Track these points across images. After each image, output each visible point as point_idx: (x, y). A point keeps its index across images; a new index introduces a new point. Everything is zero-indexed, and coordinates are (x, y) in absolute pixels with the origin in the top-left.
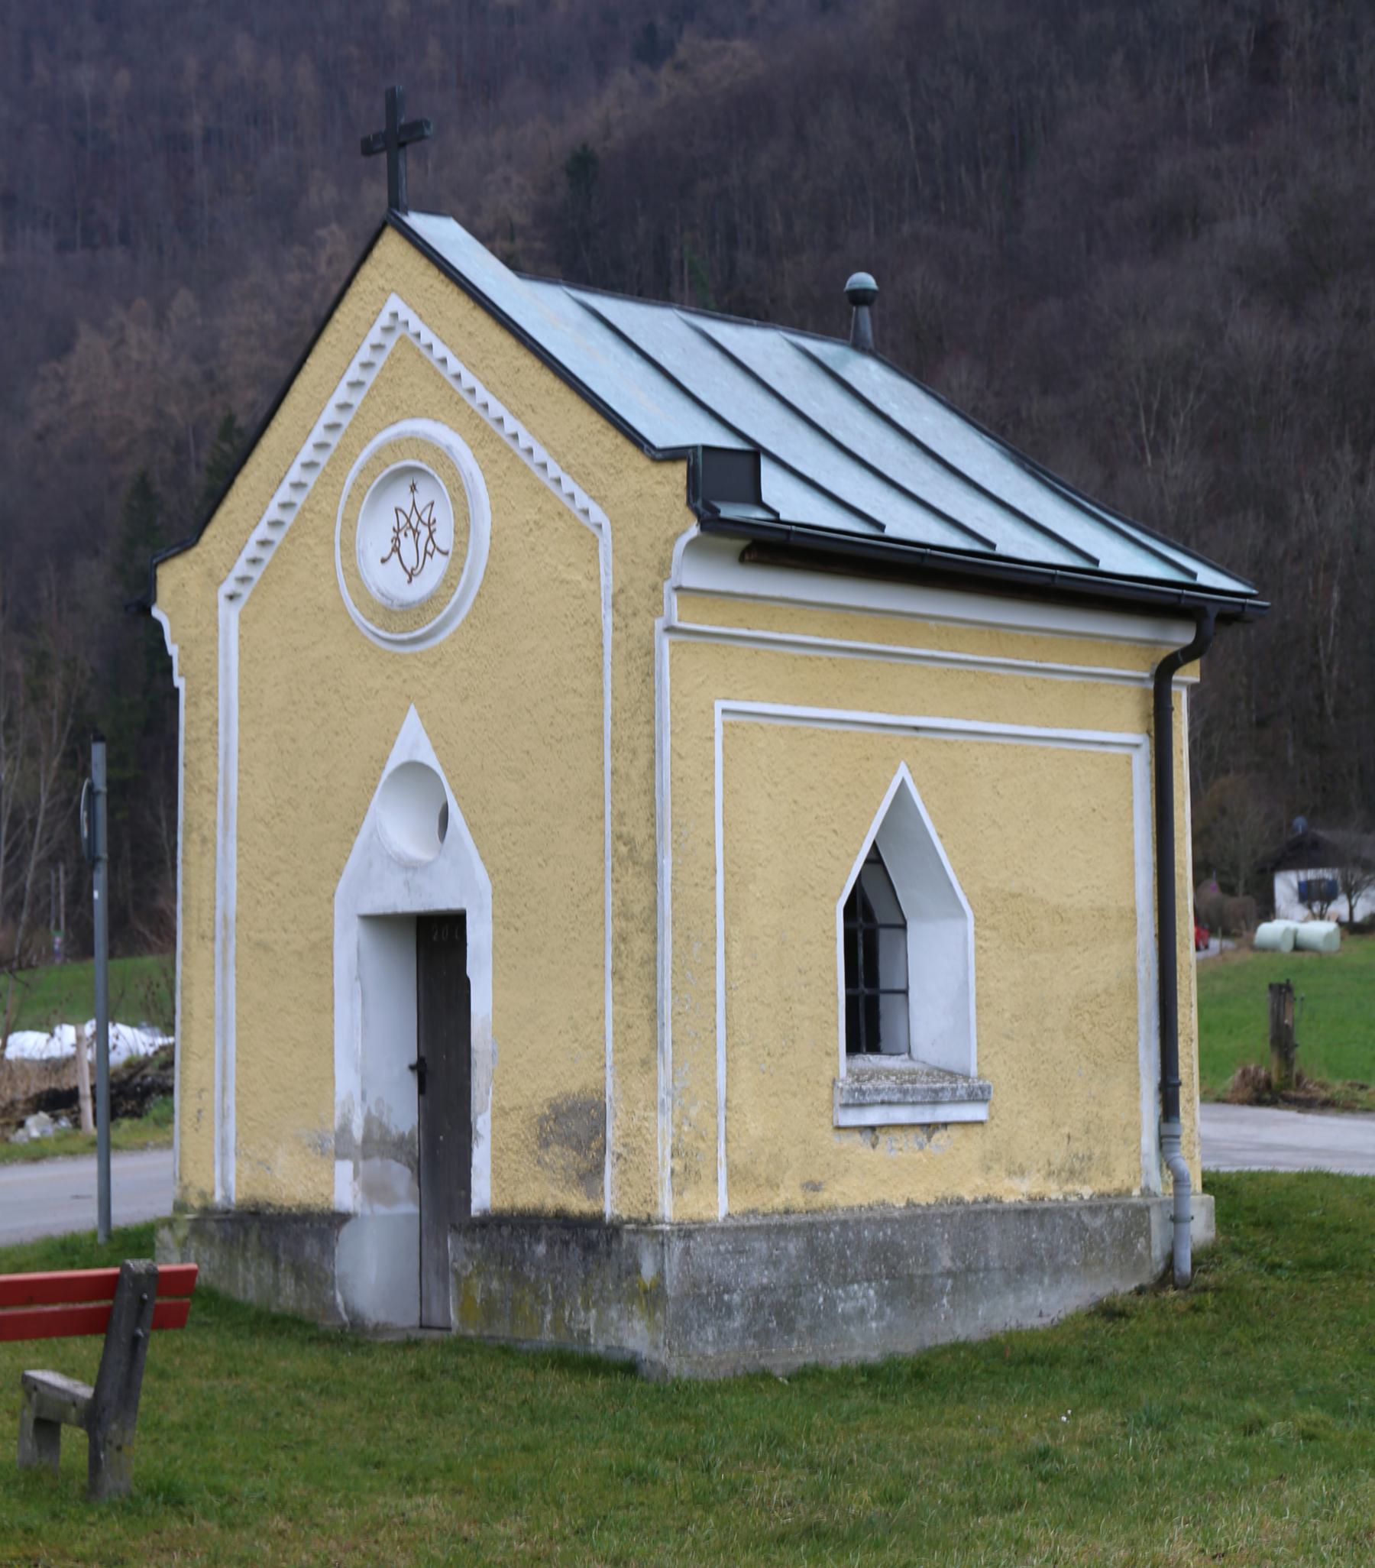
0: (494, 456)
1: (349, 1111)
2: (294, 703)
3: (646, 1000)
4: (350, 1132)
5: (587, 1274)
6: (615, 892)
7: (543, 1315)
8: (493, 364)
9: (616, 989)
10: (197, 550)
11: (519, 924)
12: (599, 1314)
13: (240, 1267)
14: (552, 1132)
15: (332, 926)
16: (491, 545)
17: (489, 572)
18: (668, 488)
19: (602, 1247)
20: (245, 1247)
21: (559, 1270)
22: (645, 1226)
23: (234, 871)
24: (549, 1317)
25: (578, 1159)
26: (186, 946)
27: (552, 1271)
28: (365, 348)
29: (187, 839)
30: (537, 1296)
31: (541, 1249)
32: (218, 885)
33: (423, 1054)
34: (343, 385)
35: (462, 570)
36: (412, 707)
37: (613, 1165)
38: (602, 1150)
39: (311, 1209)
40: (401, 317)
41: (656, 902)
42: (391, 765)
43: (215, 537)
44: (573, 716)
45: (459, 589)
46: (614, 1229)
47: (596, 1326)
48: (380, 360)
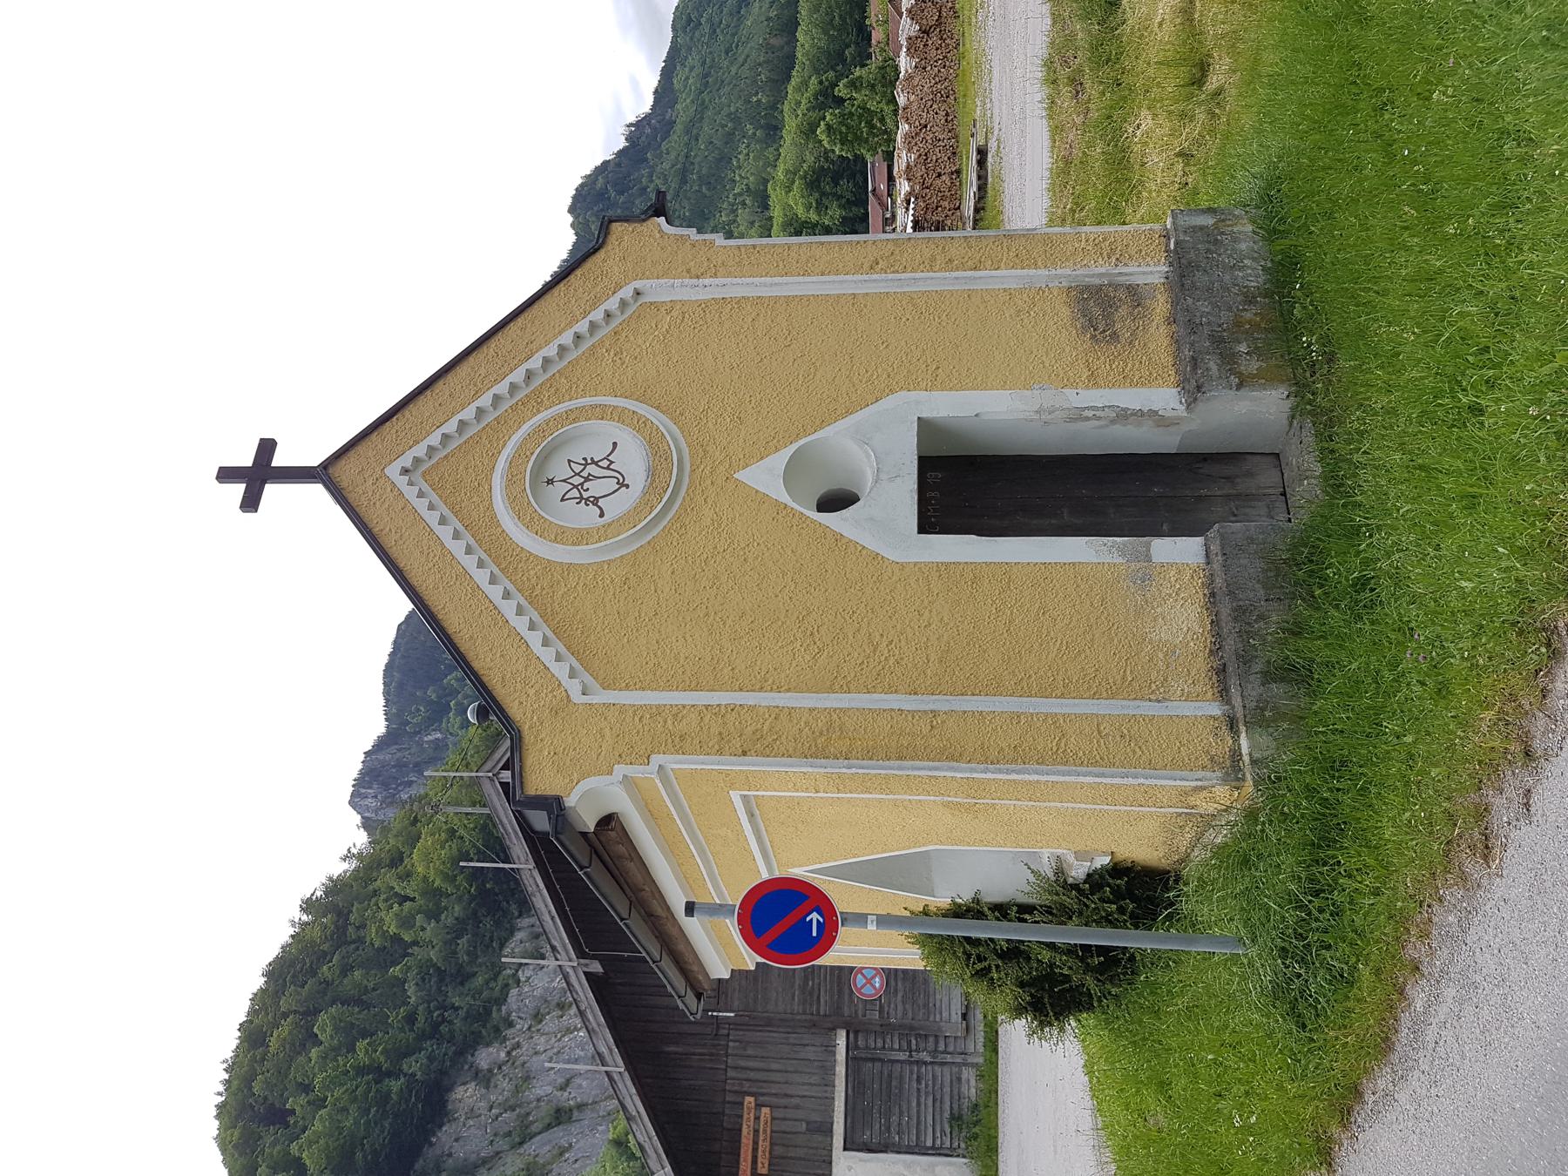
16: (621, 396)
40: (408, 464)
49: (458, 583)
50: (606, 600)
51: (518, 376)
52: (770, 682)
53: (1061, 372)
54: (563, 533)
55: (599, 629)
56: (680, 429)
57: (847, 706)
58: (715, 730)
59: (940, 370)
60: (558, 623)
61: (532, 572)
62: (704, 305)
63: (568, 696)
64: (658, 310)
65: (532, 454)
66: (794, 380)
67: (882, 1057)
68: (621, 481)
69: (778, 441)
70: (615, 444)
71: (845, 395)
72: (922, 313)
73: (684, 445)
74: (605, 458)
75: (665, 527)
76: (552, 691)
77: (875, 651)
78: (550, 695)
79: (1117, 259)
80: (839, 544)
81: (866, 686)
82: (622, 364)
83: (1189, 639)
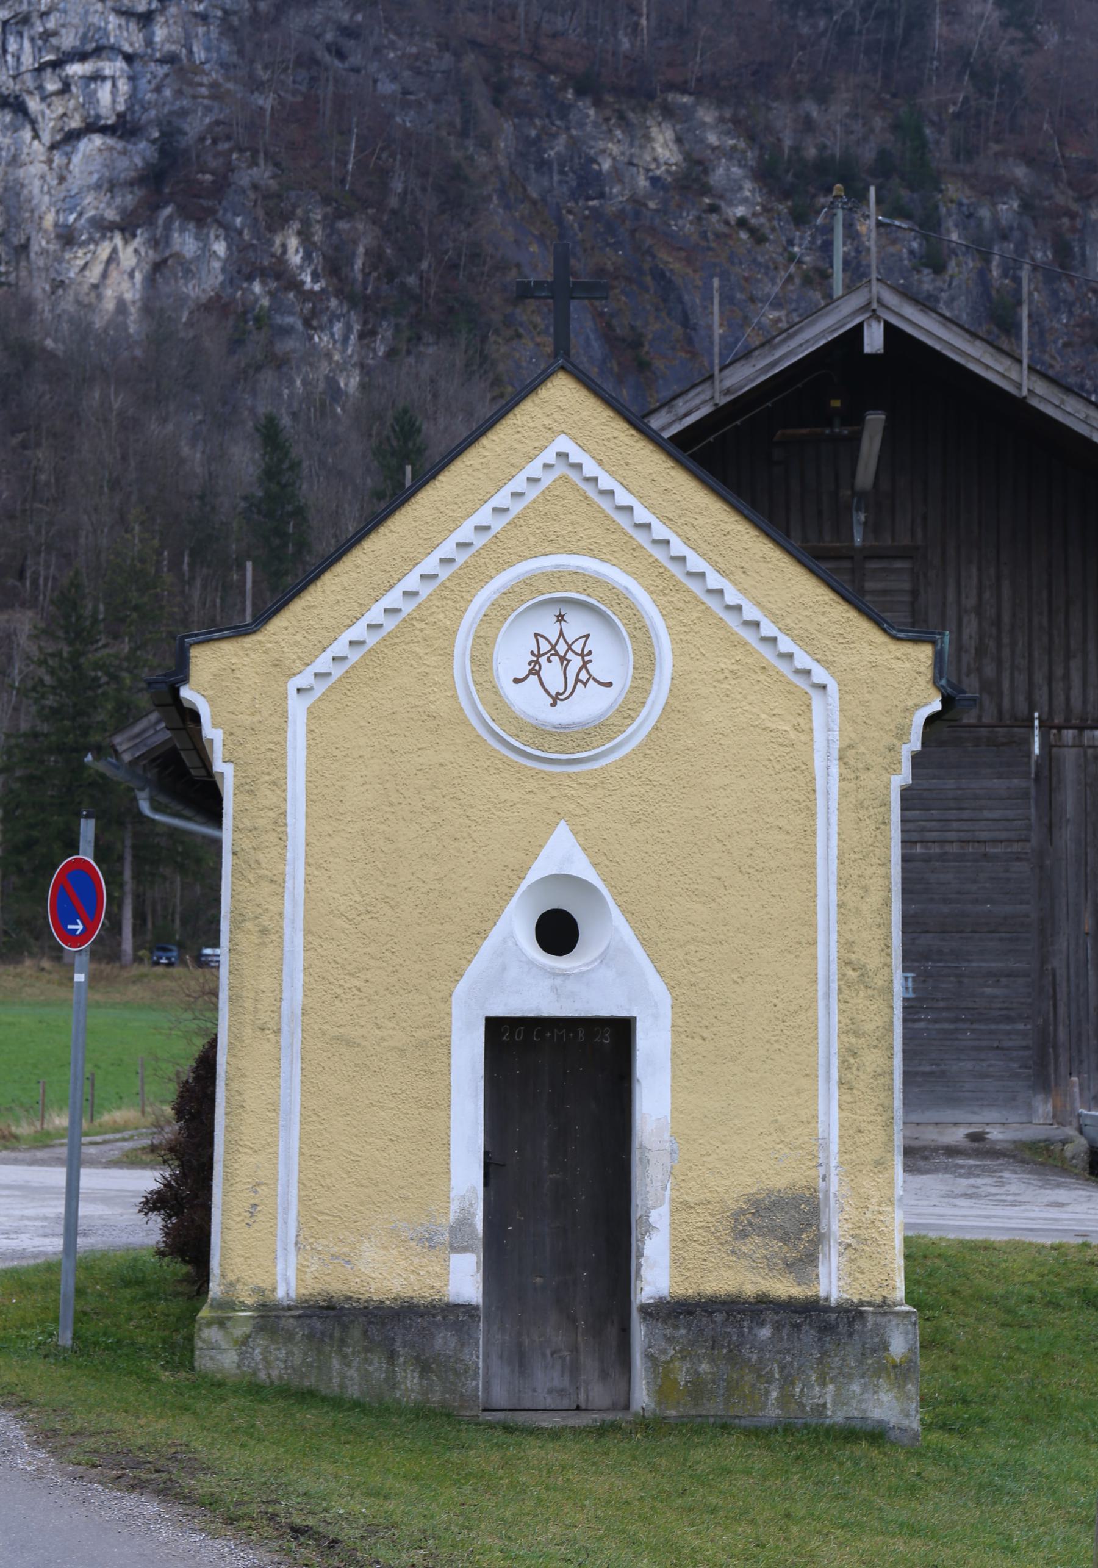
0: (681, 605)
1: (471, 1205)
2: (391, 804)
3: (880, 1108)
5: (824, 1353)
6: (841, 1012)
7: (767, 1393)
8: (695, 523)
9: (844, 1097)
12: (838, 1389)
13: (336, 1363)
14: (751, 1224)
15: (449, 1025)
16: (673, 684)
17: (667, 708)
18: (908, 665)
19: (842, 1328)
20: (342, 1341)
21: (788, 1351)
25: (785, 1249)
27: (779, 1352)
28: (521, 478)
30: (759, 1376)
31: (765, 1333)
34: (487, 508)
35: (644, 703)
36: (562, 823)
37: (841, 1255)
38: (819, 1240)
39: (415, 1301)
43: (286, 628)
45: (638, 721)
47: (834, 1401)
48: (533, 493)
49: (421, 541)
50: (410, 699)
51: (696, 563)
52: (316, 873)
53: (694, 1174)
55: (375, 694)
56: (627, 756)
57: (286, 949)
58: (260, 823)
59: (701, 1041)
61: (441, 616)
62: (805, 769)
63: (294, 675)
65: (588, 595)
69: (607, 866)
70: (609, 684)
71: (667, 936)
73: (603, 762)
75: (498, 752)
76: (300, 658)
77: (350, 974)
78: (295, 657)
79: (850, 1245)
80: (474, 936)
82: (719, 681)
83: (363, 1278)
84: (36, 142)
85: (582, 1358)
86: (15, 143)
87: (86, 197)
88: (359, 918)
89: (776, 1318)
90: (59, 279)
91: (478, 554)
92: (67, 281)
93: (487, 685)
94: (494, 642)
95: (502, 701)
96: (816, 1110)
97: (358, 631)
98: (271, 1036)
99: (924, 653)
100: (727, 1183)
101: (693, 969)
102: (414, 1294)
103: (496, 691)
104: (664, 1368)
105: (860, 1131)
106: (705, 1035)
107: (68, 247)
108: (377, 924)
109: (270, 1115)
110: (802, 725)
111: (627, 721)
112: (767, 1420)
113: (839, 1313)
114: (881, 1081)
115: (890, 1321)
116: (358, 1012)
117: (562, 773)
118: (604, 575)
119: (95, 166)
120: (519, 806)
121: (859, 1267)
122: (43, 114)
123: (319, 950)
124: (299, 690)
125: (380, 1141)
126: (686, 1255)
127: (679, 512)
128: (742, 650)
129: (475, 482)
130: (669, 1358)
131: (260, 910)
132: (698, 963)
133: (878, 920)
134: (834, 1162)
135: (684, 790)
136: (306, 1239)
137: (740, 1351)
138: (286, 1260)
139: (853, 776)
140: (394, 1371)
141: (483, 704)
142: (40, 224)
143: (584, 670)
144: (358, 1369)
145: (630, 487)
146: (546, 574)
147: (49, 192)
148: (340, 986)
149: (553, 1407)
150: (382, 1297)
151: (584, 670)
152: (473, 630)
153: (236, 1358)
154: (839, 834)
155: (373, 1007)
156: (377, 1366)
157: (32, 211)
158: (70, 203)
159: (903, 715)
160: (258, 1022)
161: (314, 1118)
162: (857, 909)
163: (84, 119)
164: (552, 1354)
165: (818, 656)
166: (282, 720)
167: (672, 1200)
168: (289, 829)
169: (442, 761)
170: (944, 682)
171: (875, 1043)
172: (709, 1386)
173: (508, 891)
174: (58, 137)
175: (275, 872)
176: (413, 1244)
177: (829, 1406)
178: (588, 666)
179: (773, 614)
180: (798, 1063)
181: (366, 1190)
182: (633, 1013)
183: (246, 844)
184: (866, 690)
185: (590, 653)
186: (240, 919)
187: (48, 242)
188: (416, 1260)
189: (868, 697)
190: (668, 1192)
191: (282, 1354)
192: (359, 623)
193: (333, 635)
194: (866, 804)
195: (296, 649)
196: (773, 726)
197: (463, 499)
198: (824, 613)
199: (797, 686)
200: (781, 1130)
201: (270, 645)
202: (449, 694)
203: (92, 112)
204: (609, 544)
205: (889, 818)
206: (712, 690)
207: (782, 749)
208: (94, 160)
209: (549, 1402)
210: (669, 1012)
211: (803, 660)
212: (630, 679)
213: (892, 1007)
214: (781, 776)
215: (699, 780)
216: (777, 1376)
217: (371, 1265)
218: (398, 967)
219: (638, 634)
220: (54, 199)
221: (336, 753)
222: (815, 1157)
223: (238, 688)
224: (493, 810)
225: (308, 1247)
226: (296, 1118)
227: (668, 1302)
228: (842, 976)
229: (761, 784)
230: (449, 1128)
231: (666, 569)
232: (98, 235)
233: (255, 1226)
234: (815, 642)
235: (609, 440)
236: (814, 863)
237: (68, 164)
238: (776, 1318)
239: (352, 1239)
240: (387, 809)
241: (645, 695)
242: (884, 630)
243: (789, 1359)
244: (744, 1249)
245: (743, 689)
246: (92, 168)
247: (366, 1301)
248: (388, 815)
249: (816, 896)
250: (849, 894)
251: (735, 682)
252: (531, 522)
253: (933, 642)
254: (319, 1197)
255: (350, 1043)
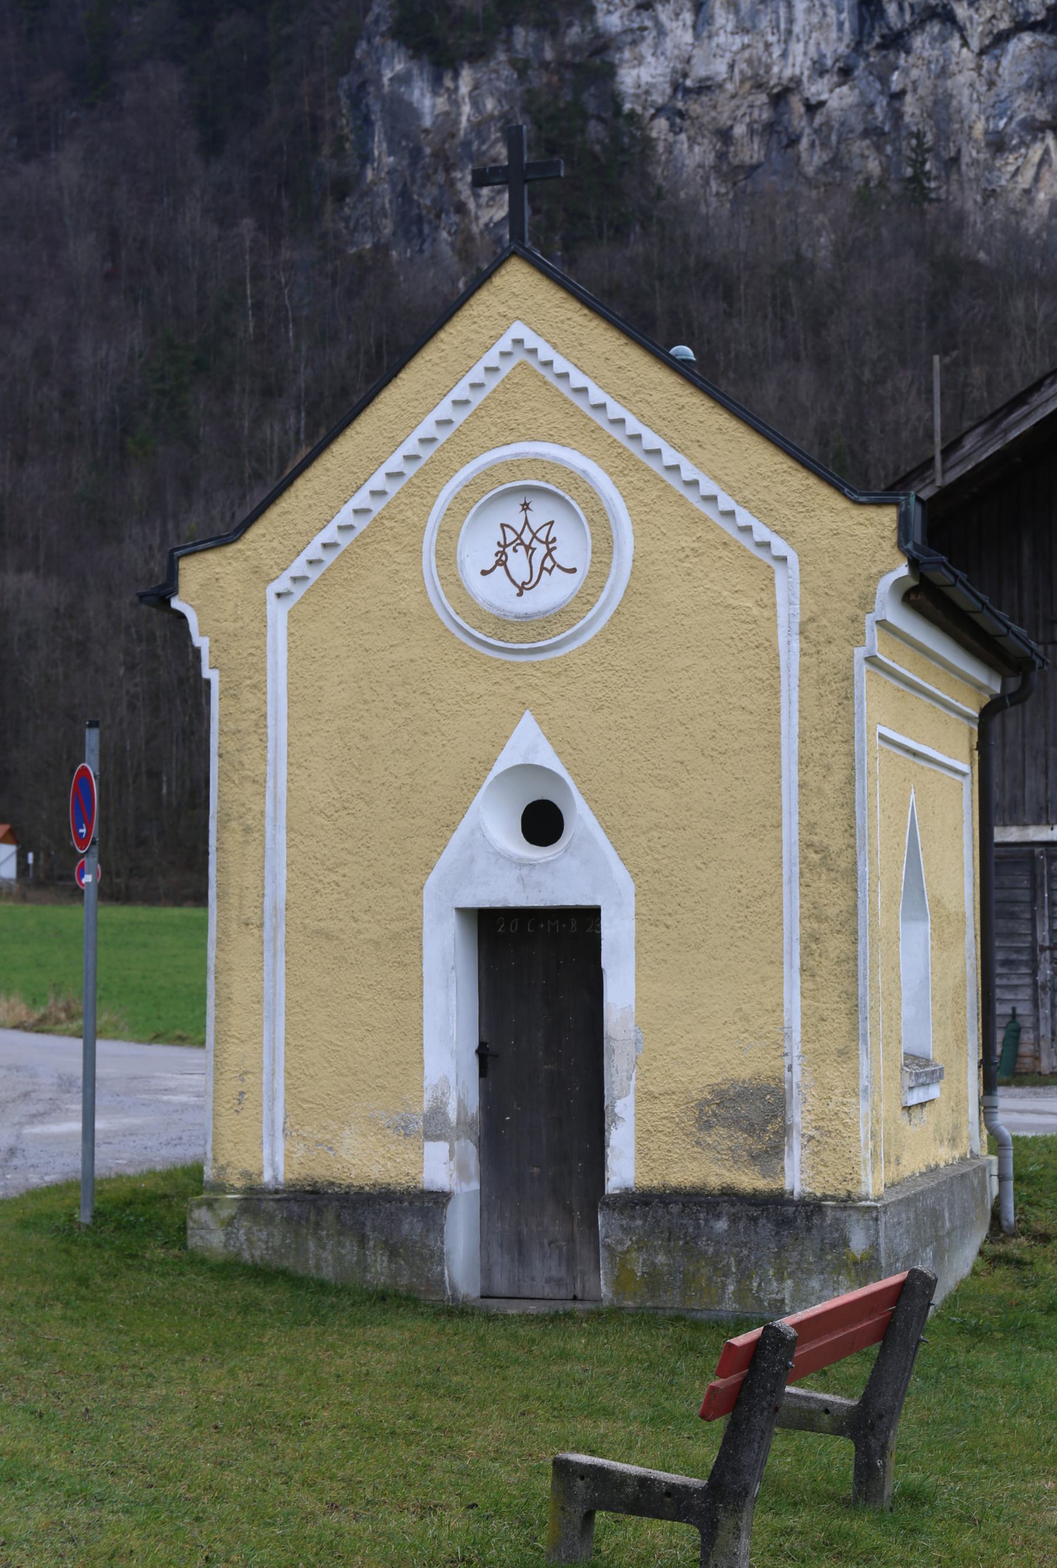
0: (641, 484)
1: (443, 1094)
2: (366, 702)
3: (844, 995)
4: (444, 1114)
5: (782, 1248)
6: (803, 896)
7: (724, 1286)
8: (650, 399)
9: (806, 985)
10: (238, 546)
11: (669, 921)
12: (796, 1284)
13: (312, 1245)
14: (715, 1115)
15: (421, 918)
16: (634, 567)
17: (630, 592)
18: (871, 530)
20: (318, 1225)
21: (745, 1244)
22: (847, 1202)
23: (283, 861)
24: (731, 1288)
25: (750, 1141)
26: (223, 932)
28: (479, 368)
29: (223, 825)
30: (716, 1269)
31: (722, 1225)
32: (267, 873)
33: (485, 1040)
34: (447, 402)
35: (602, 587)
36: (527, 713)
37: (803, 1147)
38: (785, 1131)
39: (392, 1187)
41: (856, 906)
42: (499, 768)
43: (264, 535)
44: (740, 731)
46: (812, 1207)
47: (792, 1296)
48: (493, 383)
49: (385, 440)
50: (382, 597)
52: (297, 772)
54: (451, 538)
55: (350, 595)
56: (589, 643)
57: (267, 847)
58: (243, 725)
60: (355, 553)
62: (769, 646)
63: (272, 580)
64: (762, 590)
65: (547, 481)
66: (654, 764)
67: (1039, 902)
68: (527, 586)
69: (570, 754)
70: (573, 571)
71: (630, 823)
72: (748, 907)
74: (555, 562)
75: (465, 644)
76: (277, 564)
77: (329, 870)
78: (272, 563)
79: (812, 1138)
81: (293, 862)
82: (680, 560)
84: (965, 50)
85: (578, 1248)
86: (944, 54)
87: (1016, 100)
88: (336, 815)
89: (733, 1210)
90: (990, 188)
91: (442, 449)
92: (998, 190)
93: (452, 579)
94: (458, 535)
95: (466, 594)
96: (781, 998)
97: (329, 534)
98: (255, 931)
99: (888, 516)
100: (692, 1073)
101: (656, 856)
102: (390, 1181)
103: (459, 584)
104: (621, 1259)
105: (823, 1020)
106: (668, 923)
107: (998, 155)
108: (353, 820)
109: (255, 1006)
110: (765, 600)
111: (588, 606)
112: (724, 1314)
113: (797, 1207)
114: (845, 967)
115: (850, 1216)
116: (336, 906)
117: (527, 663)
118: (561, 460)
119: (1025, 66)
120: (485, 697)
121: (822, 1160)
122: (971, 19)
123: (301, 847)
124: (279, 595)
125: (358, 1032)
126: (651, 1145)
127: (634, 389)
128: (702, 527)
129: (436, 377)
130: (625, 1248)
131: (244, 810)
132: (662, 850)
133: (841, 800)
134: (796, 1052)
135: (646, 674)
136: (292, 1126)
137: (696, 1243)
138: (272, 1146)
139: (814, 650)
140: (364, 1254)
141: (447, 597)
142: (969, 134)
143: (548, 558)
144: (332, 1251)
145: (584, 369)
146: (505, 463)
147: (978, 100)
148: (320, 881)
149: (551, 1296)
150: (362, 1183)
151: (548, 558)
152: (438, 525)
153: (223, 1238)
154: (800, 712)
155: (350, 901)
156: (349, 1249)
157: (962, 122)
158: (1000, 108)
159: (866, 583)
160: (243, 917)
161: (298, 1010)
162: (819, 788)
163: (1013, 19)
164: (550, 1244)
165: (777, 528)
166: (262, 625)
167: (637, 1090)
168: (269, 731)
169: (412, 657)
170: (910, 546)
171: (839, 927)
172: (666, 1278)
173: (475, 783)
174: (987, 42)
175: (257, 772)
176: (389, 1131)
177: (787, 1301)
178: (553, 553)
179: (730, 487)
180: (762, 950)
181: (346, 1079)
182: (598, 903)
183: (231, 746)
184: (827, 559)
185: (554, 540)
186: (226, 818)
187: (978, 152)
188: (393, 1148)
189: (830, 566)
190: (633, 1082)
191: (264, 1235)
192: (330, 525)
193: (306, 539)
194: (828, 678)
195: (273, 555)
196: (735, 603)
197: (423, 395)
198: (782, 482)
199: (760, 560)
200: (746, 1019)
201: (249, 553)
202: (418, 590)
203: (1021, 10)
204: (568, 427)
205: (852, 693)
206: (674, 570)
207: (745, 626)
208: (1024, 59)
209: (547, 1291)
210: (632, 899)
211: (762, 533)
212: (588, 564)
213: (856, 890)
214: (744, 654)
215: (662, 663)
216: (734, 1270)
217: (351, 1152)
218: (373, 862)
219: (596, 517)
220: (983, 106)
221: (314, 654)
222: (780, 1046)
223: (222, 597)
224: (461, 703)
225: (294, 1134)
226: (281, 1009)
227: (633, 1193)
228: (804, 859)
229: (723, 664)
230: (421, 1018)
231: (625, 449)
232: (1029, 138)
233: (243, 1113)
234: (773, 513)
235: (562, 322)
236: (779, 743)
237: (997, 68)
238: (733, 1210)
239: (334, 1126)
240: (361, 706)
241: (603, 579)
242: (845, 495)
243: (745, 1252)
244: (709, 1140)
245: (705, 567)
246: (1022, 69)
247: (348, 1187)
248: (362, 713)
249: (781, 777)
250: (811, 773)
251: (697, 560)
252: (492, 412)
253: (897, 504)
254: (303, 1086)
255: (328, 936)
